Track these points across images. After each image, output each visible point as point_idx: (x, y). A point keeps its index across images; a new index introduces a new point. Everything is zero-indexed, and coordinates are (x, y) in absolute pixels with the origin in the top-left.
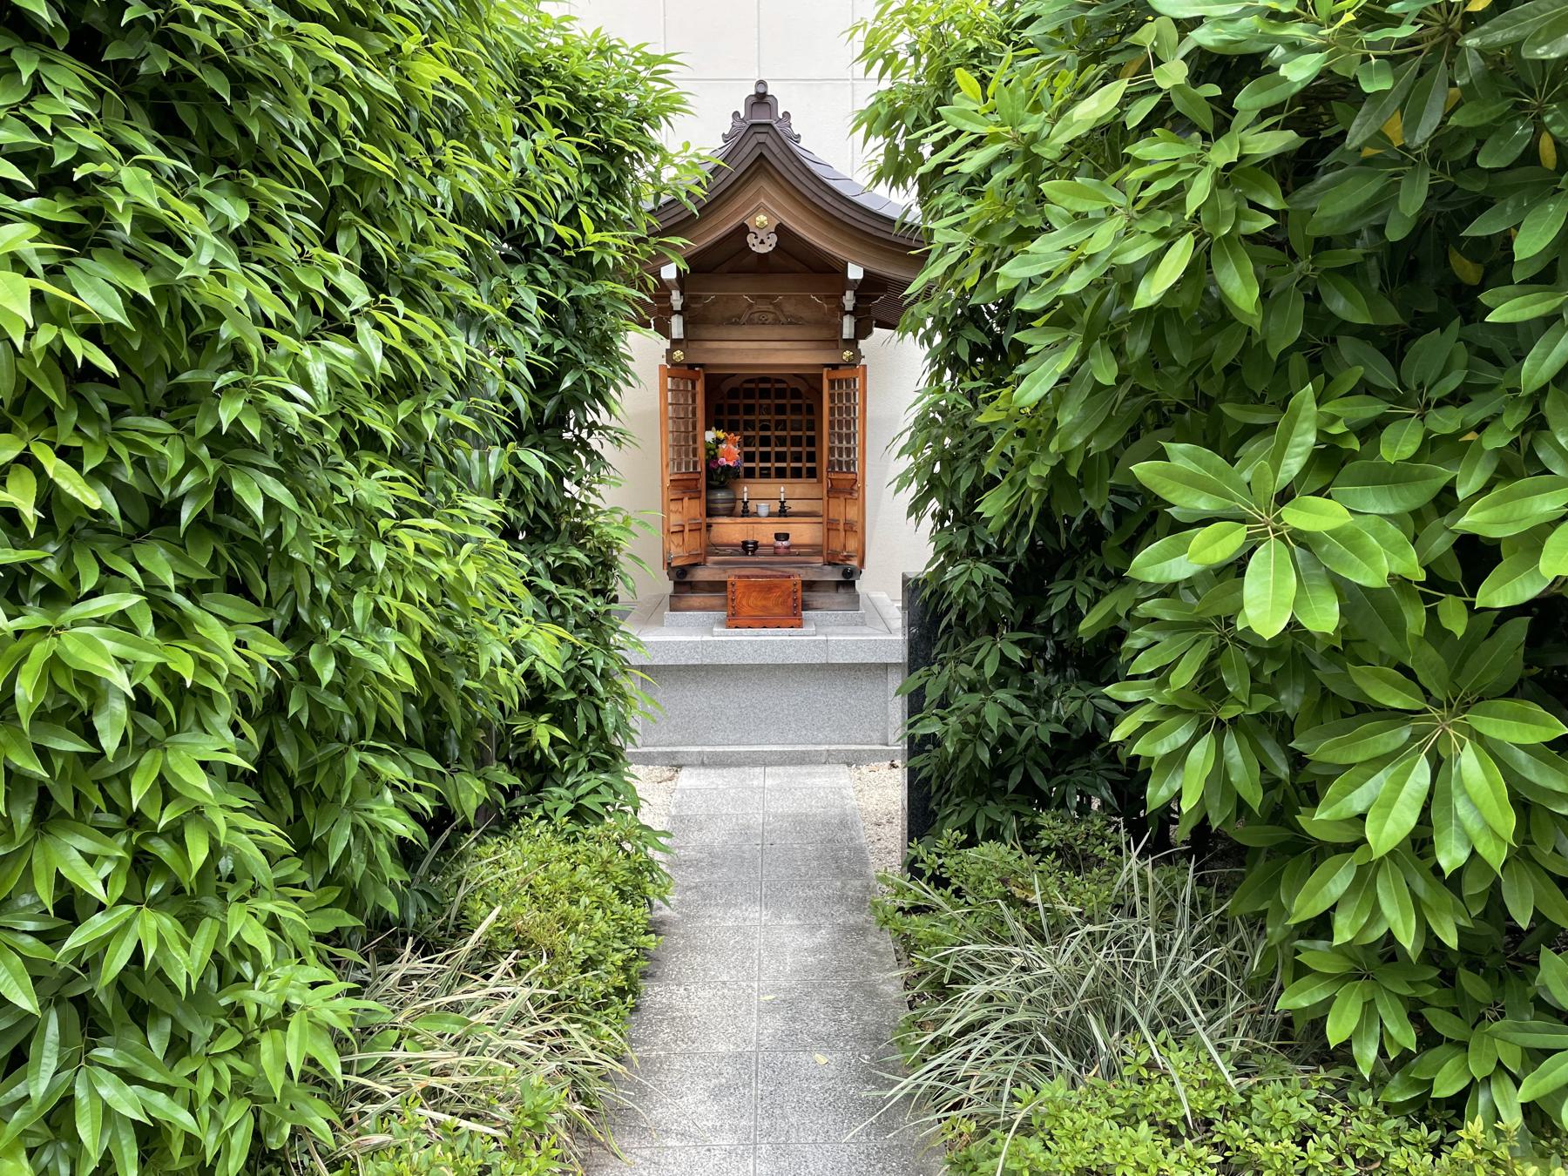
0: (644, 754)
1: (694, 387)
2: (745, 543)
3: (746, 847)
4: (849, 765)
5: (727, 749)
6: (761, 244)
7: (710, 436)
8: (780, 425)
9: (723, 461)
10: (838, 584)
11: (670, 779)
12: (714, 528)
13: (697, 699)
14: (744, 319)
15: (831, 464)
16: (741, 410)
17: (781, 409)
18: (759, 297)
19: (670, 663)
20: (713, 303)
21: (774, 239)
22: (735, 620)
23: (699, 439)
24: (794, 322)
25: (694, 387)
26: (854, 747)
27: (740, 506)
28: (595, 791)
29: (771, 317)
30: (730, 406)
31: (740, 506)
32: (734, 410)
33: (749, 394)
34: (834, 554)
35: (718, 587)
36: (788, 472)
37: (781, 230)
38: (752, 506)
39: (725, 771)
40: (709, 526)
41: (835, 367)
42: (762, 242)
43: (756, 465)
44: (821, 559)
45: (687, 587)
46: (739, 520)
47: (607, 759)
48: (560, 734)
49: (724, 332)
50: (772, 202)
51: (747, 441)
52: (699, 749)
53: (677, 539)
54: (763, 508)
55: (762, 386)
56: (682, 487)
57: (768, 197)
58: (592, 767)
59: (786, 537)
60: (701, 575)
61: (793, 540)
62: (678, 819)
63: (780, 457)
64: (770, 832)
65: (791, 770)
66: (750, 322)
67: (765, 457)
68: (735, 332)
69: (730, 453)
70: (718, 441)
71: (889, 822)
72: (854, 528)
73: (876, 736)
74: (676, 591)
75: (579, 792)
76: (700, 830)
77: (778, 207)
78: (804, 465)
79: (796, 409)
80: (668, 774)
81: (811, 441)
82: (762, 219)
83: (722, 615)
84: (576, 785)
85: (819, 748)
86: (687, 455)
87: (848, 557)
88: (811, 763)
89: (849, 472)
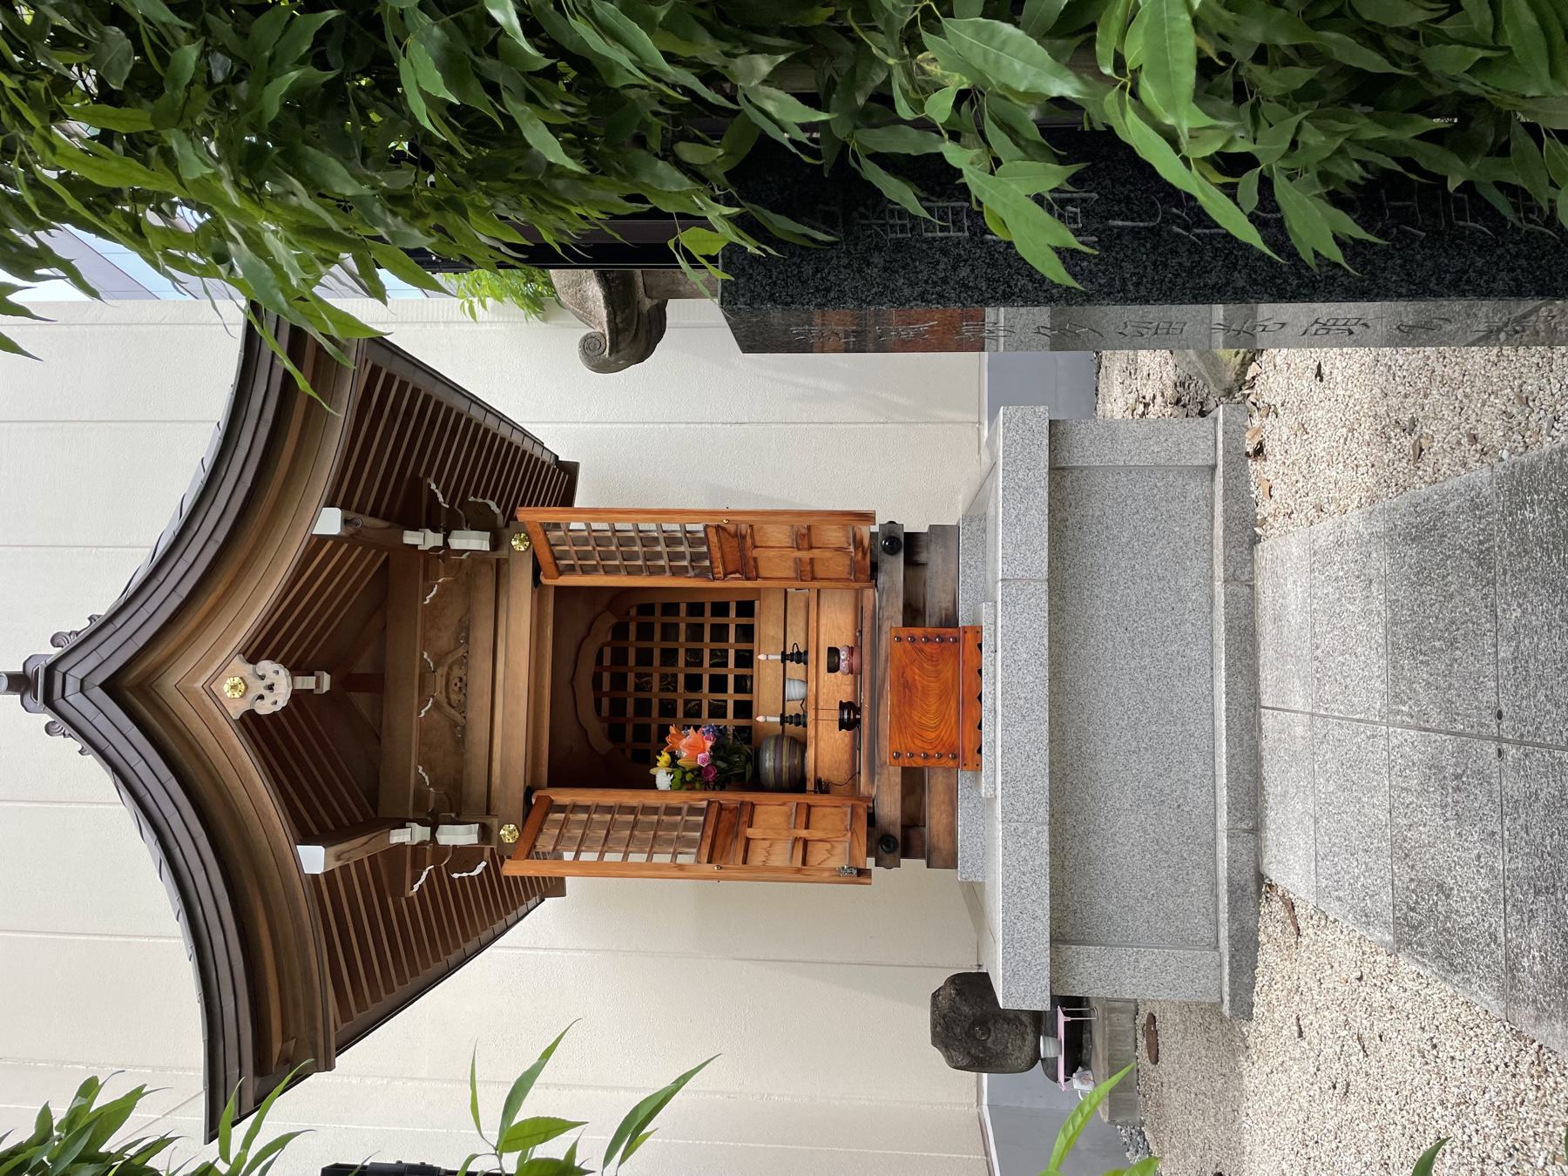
3: (1515, 787)
4: (1255, 540)
5: (1223, 780)
6: (276, 688)
7: (663, 779)
8: (669, 656)
9: (702, 758)
10: (912, 563)
11: (1291, 907)
13: (1125, 833)
14: (458, 717)
16: (643, 720)
17: (645, 658)
18: (422, 687)
19: (1046, 887)
20: (429, 769)
21: (266, 666)
24: (464, 632)
25: (562, 809)
26: (1219, 531)
29: (457, 672)
33: (618, 707)
34: (855, 568)
35: (913, 782)
37: (253, 655)
39: (1273, 790)
41: (537, 571)
42: (271, 687)
43: (731, 697)
45: (913, 833)
46: (811, 731)
50: (201, 667)
52: (1223, 843)
53: (818, 854)
55: (606, 686)
56: (724, 841)
59: (833, 652)
60: (890, 808)
63: (720, 659)
65: (1267, 654)
66: (462, 708)
68: (478, 734)
69: (693, 745)
70: (673, 763)
71: (1411, 428)
72: (805, 529)
73: (1195, 489)
78: (733, 620)
79: (645, 632)
80: (1277, 905)
81: (696, 609)
83: (964, 777)
85: (1220, 600)
87: (858, 543)
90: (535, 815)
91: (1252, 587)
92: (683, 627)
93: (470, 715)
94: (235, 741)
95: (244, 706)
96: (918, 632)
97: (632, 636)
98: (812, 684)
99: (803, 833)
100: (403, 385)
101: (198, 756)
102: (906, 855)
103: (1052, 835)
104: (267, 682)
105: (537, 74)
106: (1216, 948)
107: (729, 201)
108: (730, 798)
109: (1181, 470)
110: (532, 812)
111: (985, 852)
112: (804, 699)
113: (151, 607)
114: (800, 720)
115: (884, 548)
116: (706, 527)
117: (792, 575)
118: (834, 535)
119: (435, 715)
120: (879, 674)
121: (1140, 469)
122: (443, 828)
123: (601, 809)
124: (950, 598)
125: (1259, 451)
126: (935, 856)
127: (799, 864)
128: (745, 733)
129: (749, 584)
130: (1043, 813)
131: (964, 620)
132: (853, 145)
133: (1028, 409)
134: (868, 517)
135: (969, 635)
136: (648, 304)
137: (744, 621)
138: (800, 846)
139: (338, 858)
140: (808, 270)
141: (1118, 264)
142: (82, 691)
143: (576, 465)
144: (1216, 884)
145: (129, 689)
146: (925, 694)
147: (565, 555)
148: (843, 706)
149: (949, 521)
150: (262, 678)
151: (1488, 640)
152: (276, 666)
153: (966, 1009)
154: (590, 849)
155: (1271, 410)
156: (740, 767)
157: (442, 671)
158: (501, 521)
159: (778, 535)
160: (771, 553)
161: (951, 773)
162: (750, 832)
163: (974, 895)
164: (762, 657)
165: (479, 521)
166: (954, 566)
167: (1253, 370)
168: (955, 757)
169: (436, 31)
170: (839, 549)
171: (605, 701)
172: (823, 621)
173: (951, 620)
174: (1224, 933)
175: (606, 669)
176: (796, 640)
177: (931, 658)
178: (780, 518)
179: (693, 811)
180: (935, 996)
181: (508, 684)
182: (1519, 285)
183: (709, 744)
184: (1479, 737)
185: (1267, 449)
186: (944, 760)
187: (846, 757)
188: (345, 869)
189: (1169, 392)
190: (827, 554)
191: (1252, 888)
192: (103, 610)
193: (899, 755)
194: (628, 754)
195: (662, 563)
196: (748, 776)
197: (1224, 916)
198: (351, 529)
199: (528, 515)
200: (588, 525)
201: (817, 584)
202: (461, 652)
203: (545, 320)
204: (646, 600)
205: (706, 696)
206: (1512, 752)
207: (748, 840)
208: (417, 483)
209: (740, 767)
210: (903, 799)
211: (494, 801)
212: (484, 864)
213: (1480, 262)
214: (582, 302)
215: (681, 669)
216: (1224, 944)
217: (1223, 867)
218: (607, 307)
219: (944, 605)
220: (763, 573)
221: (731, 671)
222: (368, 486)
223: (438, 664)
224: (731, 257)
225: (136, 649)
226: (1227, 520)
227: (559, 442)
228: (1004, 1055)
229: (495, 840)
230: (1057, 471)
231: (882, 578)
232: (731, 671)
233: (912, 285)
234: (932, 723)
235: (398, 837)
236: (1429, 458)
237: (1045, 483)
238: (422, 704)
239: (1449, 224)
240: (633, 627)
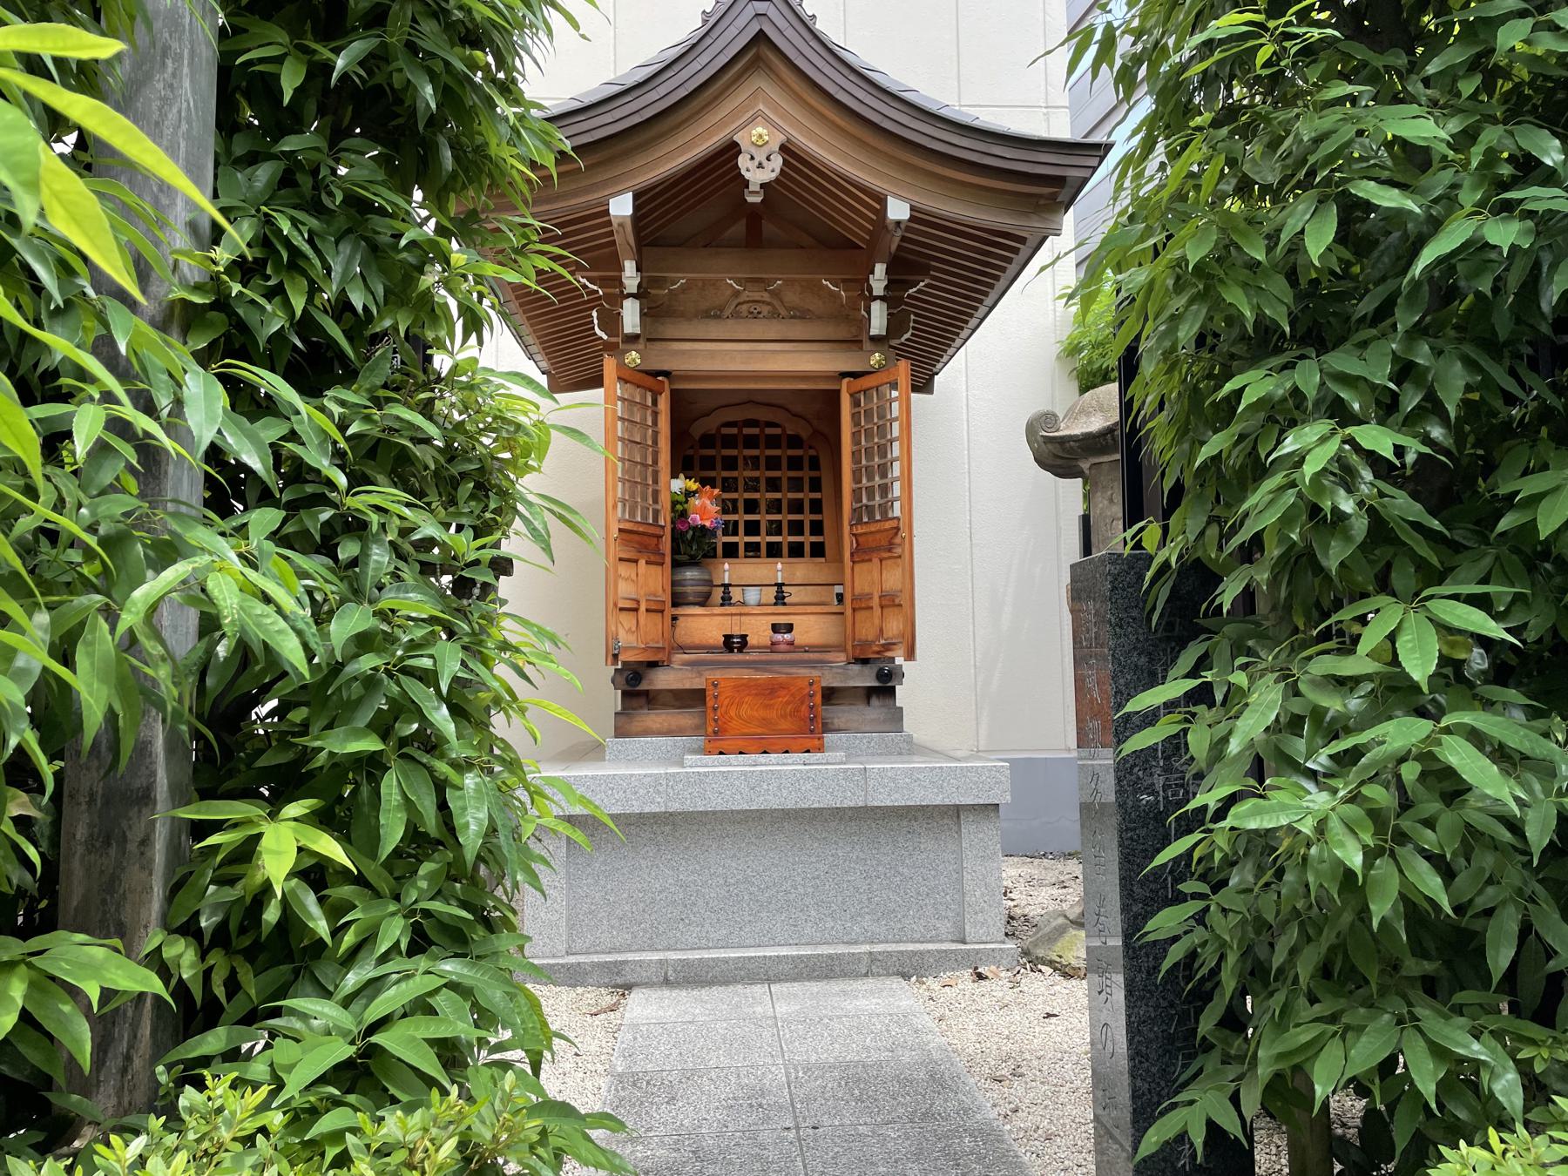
0: (568, 968)
1: (655, 402)
2: (728, 638)
3: (765, 1136)
4: (906, 976)
5: (706, 955)
6: (759, 171)
7: (678, 485)
8: (773, 485)
9: (695, 519)
10: (870, 693)
12: (681, 622)
14: (727, 312)
17: (773, 463)
20: (684, 289)
21: (777, 162)
22: (718, 741)
24: (802, 315)
25: (655, 402)
26: (911, 947)
27: (718, 593)
28: (422, 1007)
29: (765, 310)
30: (703, 458)
33: (729, 442)
34: (866, 644)
35: (693, 699)
36: (785, 550)
39: (704, 993)
42: (760, 166)
43: (741, 539)
44: (842, 657)
45: (643, 700)
47: (461, 908)
48: (330, 848)
50: (776, 108)
52: (656, 956)
53: (627, 620)
55: (746, 431)
56: (636, 542)
58: (419, 944)
60: (663, 680)
61: (798, 636)
62: (627, 1081)
63: (776, 528)
64: (807, 1100)
65: (815, 987)
66: (736, 315)
67: (752, 528)
68: (714, 329)
69: (705, 509)
70: (689, 494)
72: (899, 602)
73: (945, 927)
75: (375, 1012)
76: (672, 1100)
77: (785, 115)
78: (807, 539)
79: (795, 463)
80: (608, 1000)
83: (698, 741)
84: (373, 987)
87: (888, 646)
88: (845, 975)
89: (885, 518)
90: (649, 380)
91: (866, 975)
92: (800, 495)
94: (715, 139)
95: (744, 145)
96: (818, 699)
97: (790, 452)
98: (757, 610)
99: (643, 608)
100: (1010, 261)
101: (703, 108)
102: (624, 694)
103: (655, 815)
104: (765, 163)
105: (1255, 448)
106: (568, 953)
107: (1180, 557)
108: (666, 545)
109: (961, 915)
110: (650, 378)
111: (632, 761)
112: (744, 604)
113: (827, 70)
114: (726, 600)
115: (882, 669)
116: (898, 519)
117: (857, 591)
118: (893, 626)
119: (729, 292)
120: (777, 668)
121: (960, 880)
123: (656, 434)
124: (842, 726)
125: (980, 977)
126: (623, 718)
127: (621, 605)
128: (712, 554)
129: (847, 555)
130: (675, 807)
131: (828, 737)
132: (1217, 638)
133: (1007, 785)
134: (910, 655)
135: (817, 742)
136: (1085, 465)
137: (807, 549)
139: (620, 225)
140: (1135, 613)
141: (1146, 825)
142: (757, 15)
143: (930, 391)
144: (620, 952)
146: (767, 707)
147: (869, 399)
148: (744, 637)
149: (908, 723)
150: (768, 159)
151: (869, 1120)
154: (625, 430)
155: (1015, 984)
156: (690, 547)
157: (766, 297)
158: (894, 342)
159: (892, 579)
160: (876, 575)
161: (697, 730)
162: (642, 562)
163: (592, 751)
164: (779, 566)
165: (896, 324)
167: (1047, 970)
168: (715, 733)
169: (1281, 392)
170: (881, 630)
171: (734, 431)
173: (827, 728)
174: (582, 959)
175: (762, 431)
176: (794, 595)
177: (797, 710)
179: (656, 513)
181: (754, 352)
182: (1139, 1097)
183: (707, 524)
184: (796, 1117)
185: (983, 983)
187: (697, 642)
189: (1018, 911)
190: (877, 621)
191: (619, 981)
192: (819, 26)
194: (691, 452)
195: (864, 481)
197: (595, 958)
198: (891, 227)
199: (903, 368)
200: (896, 419)
201: (849, 612)
202: (783, 312)
203: (1058, 357)
204: (824, 462)
205: (742, 517)
206: (792, 1135)
207: (636, 561)
208: (924, 270)
209: (690, 547)
210: (671, 691)
211: (658, 345)
212: (605, 337)
213: (1154, 1070)
214: (1085, 412)
215: (764, 496)
216: (572, 959)
217: (630, 957)
220: (857, 567)
221: (763, 539)
222: (916, 231)
223: (774, 294)
224: (1140, 559)
226: (921, 953)
227: (950, 376)
229: (628, 347)
230: (956, 812)
231: (856, 668)
232: (763, 539)
233: (1126, 685)
234: (742, 713)
235: (629, 267)
236: (996, 1086)
237: (947, 802)
239: (1179, 1049)
240: (799, 452)
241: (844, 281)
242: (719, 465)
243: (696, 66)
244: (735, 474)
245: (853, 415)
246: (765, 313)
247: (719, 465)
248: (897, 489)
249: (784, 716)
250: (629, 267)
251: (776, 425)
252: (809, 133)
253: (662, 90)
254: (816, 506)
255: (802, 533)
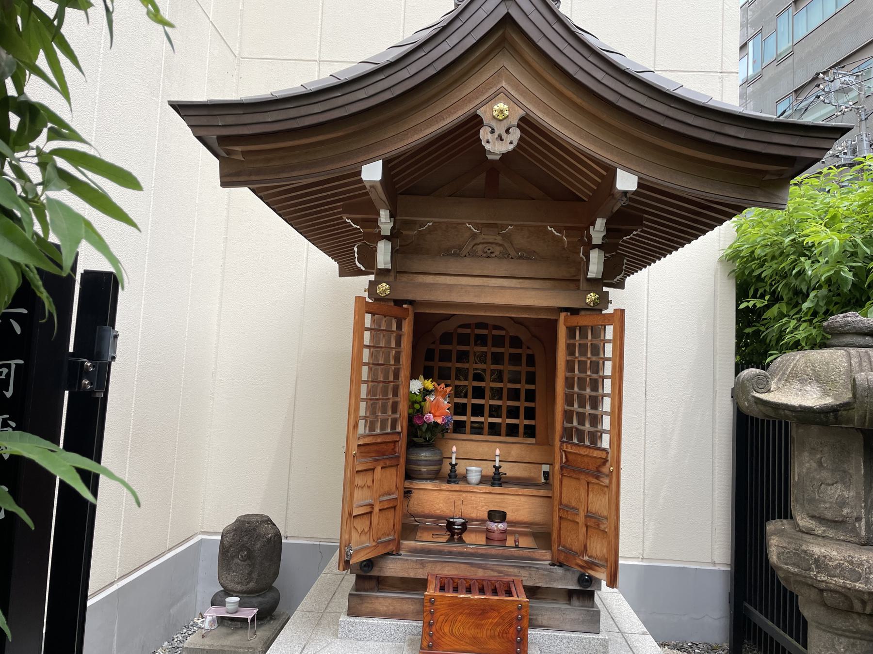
1: (399, 327)
6: (497, 144)
7: (416, 386)
9: (430, 417)
12: (415, 495)
14: (465, 251)
15: (568, 433)
20: (430, 230)
21: (516, 134)
23: (402, 391)
24: (527, 256)
25: (399, 327)
27: (447, 468)
29: (497, 250)
31: (447, 468)
32: (446, 356)
33: (464, 340)
36: (503, 430)
37: (526, 123)
38: (460, 469)
40: (408, 493)
41: (574, 311)
42: (501, 138)
44: (547, 555)
45: (373, 583)
46: (445, 486)
49: (441, 265)
50: (517, 85)
51: (458, 392)
53: (361, 525)
54: (474, 473)
55: (478, 331)
56: (372, 453)
57: (512, 80)
60: (393, 568)
63: (495, 411)
66: (472, 254)
67: (478, 410)
68: (454, 265)
69: (439, 408)
70: (426, 392)
74: (358, 587)
77: (525, 92)
78: (522, 422)
79: (515, 359)
82: (501, 113)
86: (384, 411)
90: (396, 310)
93: (467, 260)
94: (460, 113)
95: (486, 119)
104: (504, 136)
113: (568, 51)
116: (604, 450)
120: (489, 563)
122: (389, 245)
124: (545, 623)
137: (521, 430)
138: (368, 509)
145: (504, 33)
146: (478, 626)
150: (507, 131)
152: (515, 143)
153: (258, 546)
162: (379, 469)
166: (568, 627)
171: (468, 331)
172: (523, 499)
178: (613, 513)
180: (269, 521)
181: (488, 287)
183: (439, 421)
186: (428, 638)
187: (427, 511)
188: (364, 187)
190: (581, 537)
193: (432, 603)
194: (432, 347)
196: (415, 439)
198: (618, 196)
203: (721, 260)
207: (373, 470)
211: (406, 275)
218: (800, 406)
219: (540, 618)
223: (504, 236)
225: (536, 40)
228: (229, 569)
234: (455, 630)
235: (384, 216)
238: (476, 226)
241: (567, 228)
242: (455, 340)
243: (445, 47)
244: (466, 366)
245: (568, 362)
246: (497, 253)
247: (455, 340)
248: (606, 423)
249: (493, 637)
250: (384, 216)
251: (502, 329)
252: (547, 109)
253: (413, 69)
254: (531, 396)
255: (517, 417)
